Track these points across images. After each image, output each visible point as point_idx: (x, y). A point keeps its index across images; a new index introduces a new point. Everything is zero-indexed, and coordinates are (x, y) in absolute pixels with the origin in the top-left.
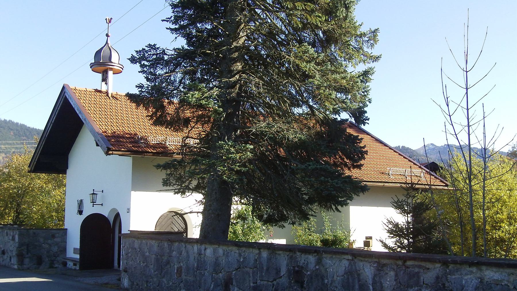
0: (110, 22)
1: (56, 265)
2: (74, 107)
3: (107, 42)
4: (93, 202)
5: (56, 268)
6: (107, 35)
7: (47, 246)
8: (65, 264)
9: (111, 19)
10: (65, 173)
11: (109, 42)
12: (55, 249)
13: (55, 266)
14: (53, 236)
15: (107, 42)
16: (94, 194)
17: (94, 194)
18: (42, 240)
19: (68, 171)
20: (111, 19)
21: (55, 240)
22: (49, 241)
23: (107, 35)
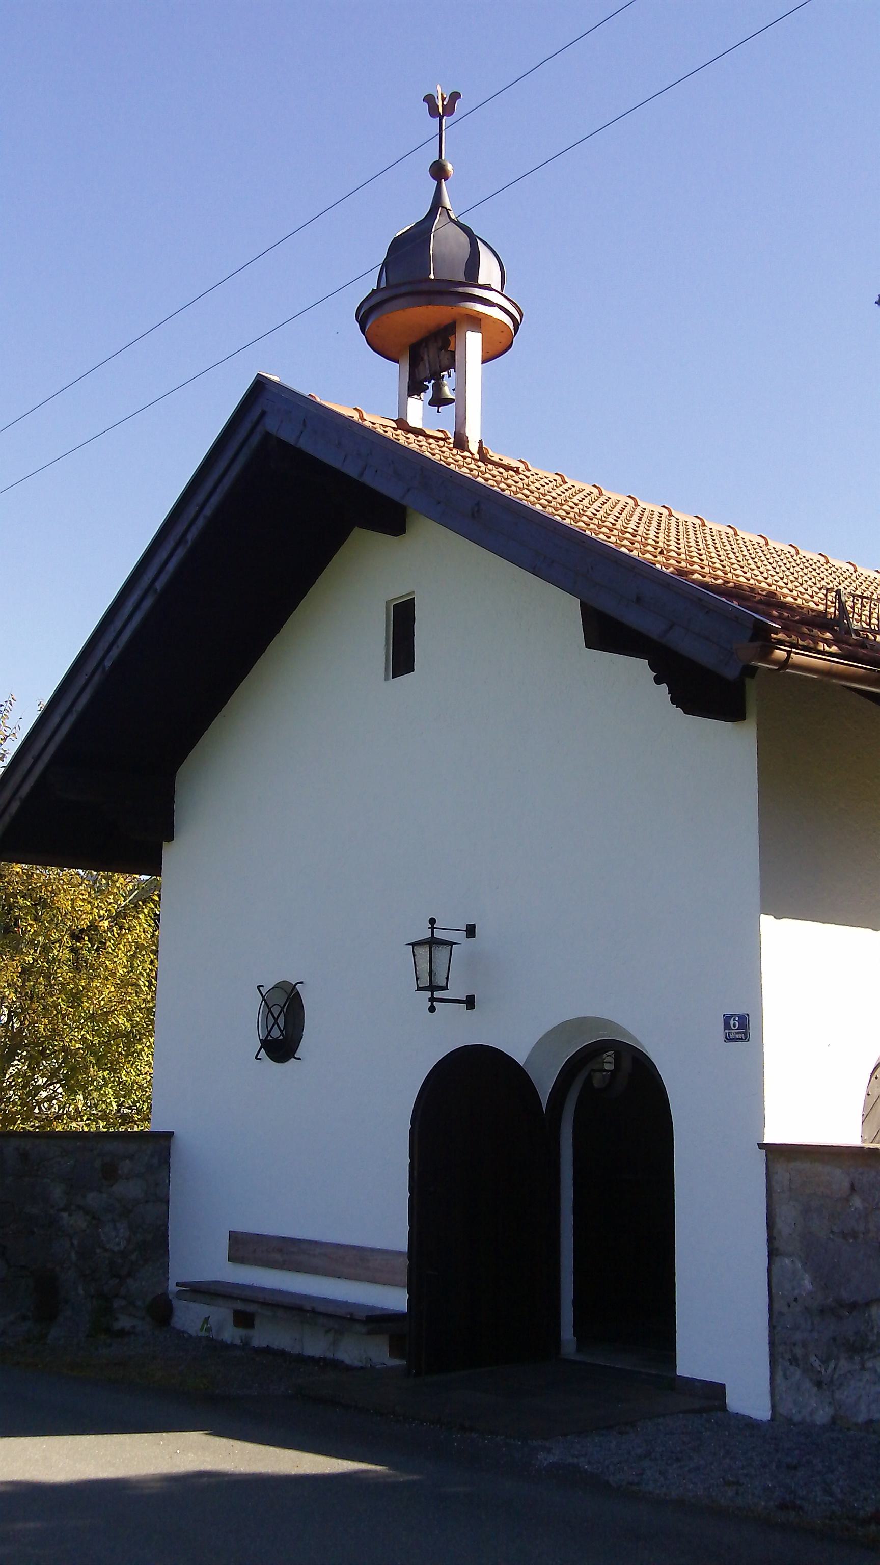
0: (449, 110)
1: (124, 1322)
2: (351, 470)
3: (437, 203)
4: (432, 988)
5: (122, 1333)
6: (438, 171)
7: (79, 1222)
8: (161, 1310)
9: (455, 96)
10: (151, 863)
11: (447, 203)
12: (116, 1237)
13: (117, 1326)
14: (110, 1173)
15: (437, 203)
16: (432, 942)
17: (432, 942)
18: (57, 1192)
19: (170, 854)
20: (455, 96)
21: (119, 1188)
22: (92, 1199)
23: (438, 171)
